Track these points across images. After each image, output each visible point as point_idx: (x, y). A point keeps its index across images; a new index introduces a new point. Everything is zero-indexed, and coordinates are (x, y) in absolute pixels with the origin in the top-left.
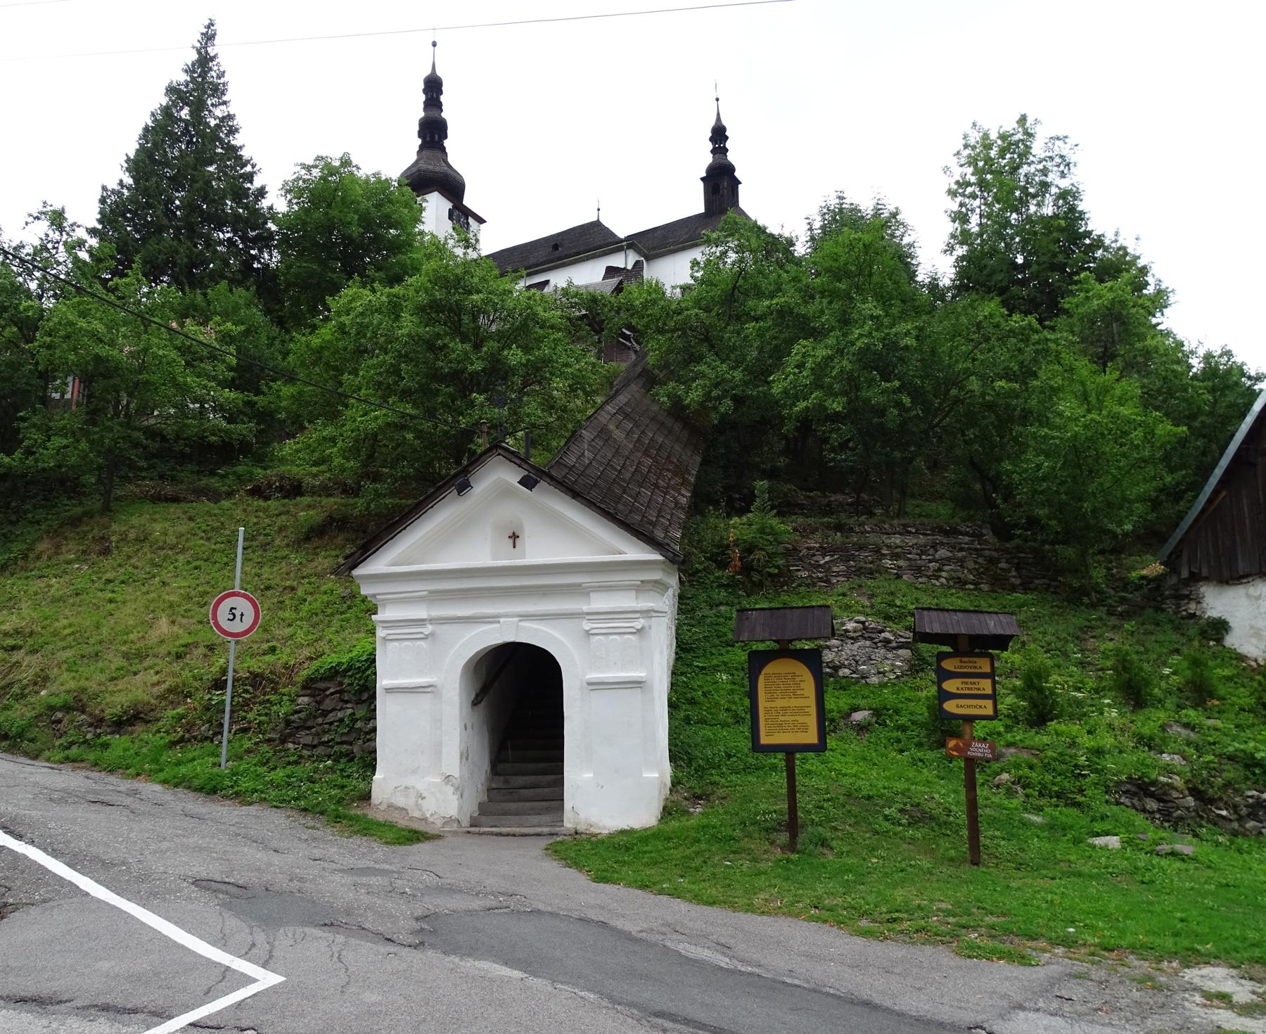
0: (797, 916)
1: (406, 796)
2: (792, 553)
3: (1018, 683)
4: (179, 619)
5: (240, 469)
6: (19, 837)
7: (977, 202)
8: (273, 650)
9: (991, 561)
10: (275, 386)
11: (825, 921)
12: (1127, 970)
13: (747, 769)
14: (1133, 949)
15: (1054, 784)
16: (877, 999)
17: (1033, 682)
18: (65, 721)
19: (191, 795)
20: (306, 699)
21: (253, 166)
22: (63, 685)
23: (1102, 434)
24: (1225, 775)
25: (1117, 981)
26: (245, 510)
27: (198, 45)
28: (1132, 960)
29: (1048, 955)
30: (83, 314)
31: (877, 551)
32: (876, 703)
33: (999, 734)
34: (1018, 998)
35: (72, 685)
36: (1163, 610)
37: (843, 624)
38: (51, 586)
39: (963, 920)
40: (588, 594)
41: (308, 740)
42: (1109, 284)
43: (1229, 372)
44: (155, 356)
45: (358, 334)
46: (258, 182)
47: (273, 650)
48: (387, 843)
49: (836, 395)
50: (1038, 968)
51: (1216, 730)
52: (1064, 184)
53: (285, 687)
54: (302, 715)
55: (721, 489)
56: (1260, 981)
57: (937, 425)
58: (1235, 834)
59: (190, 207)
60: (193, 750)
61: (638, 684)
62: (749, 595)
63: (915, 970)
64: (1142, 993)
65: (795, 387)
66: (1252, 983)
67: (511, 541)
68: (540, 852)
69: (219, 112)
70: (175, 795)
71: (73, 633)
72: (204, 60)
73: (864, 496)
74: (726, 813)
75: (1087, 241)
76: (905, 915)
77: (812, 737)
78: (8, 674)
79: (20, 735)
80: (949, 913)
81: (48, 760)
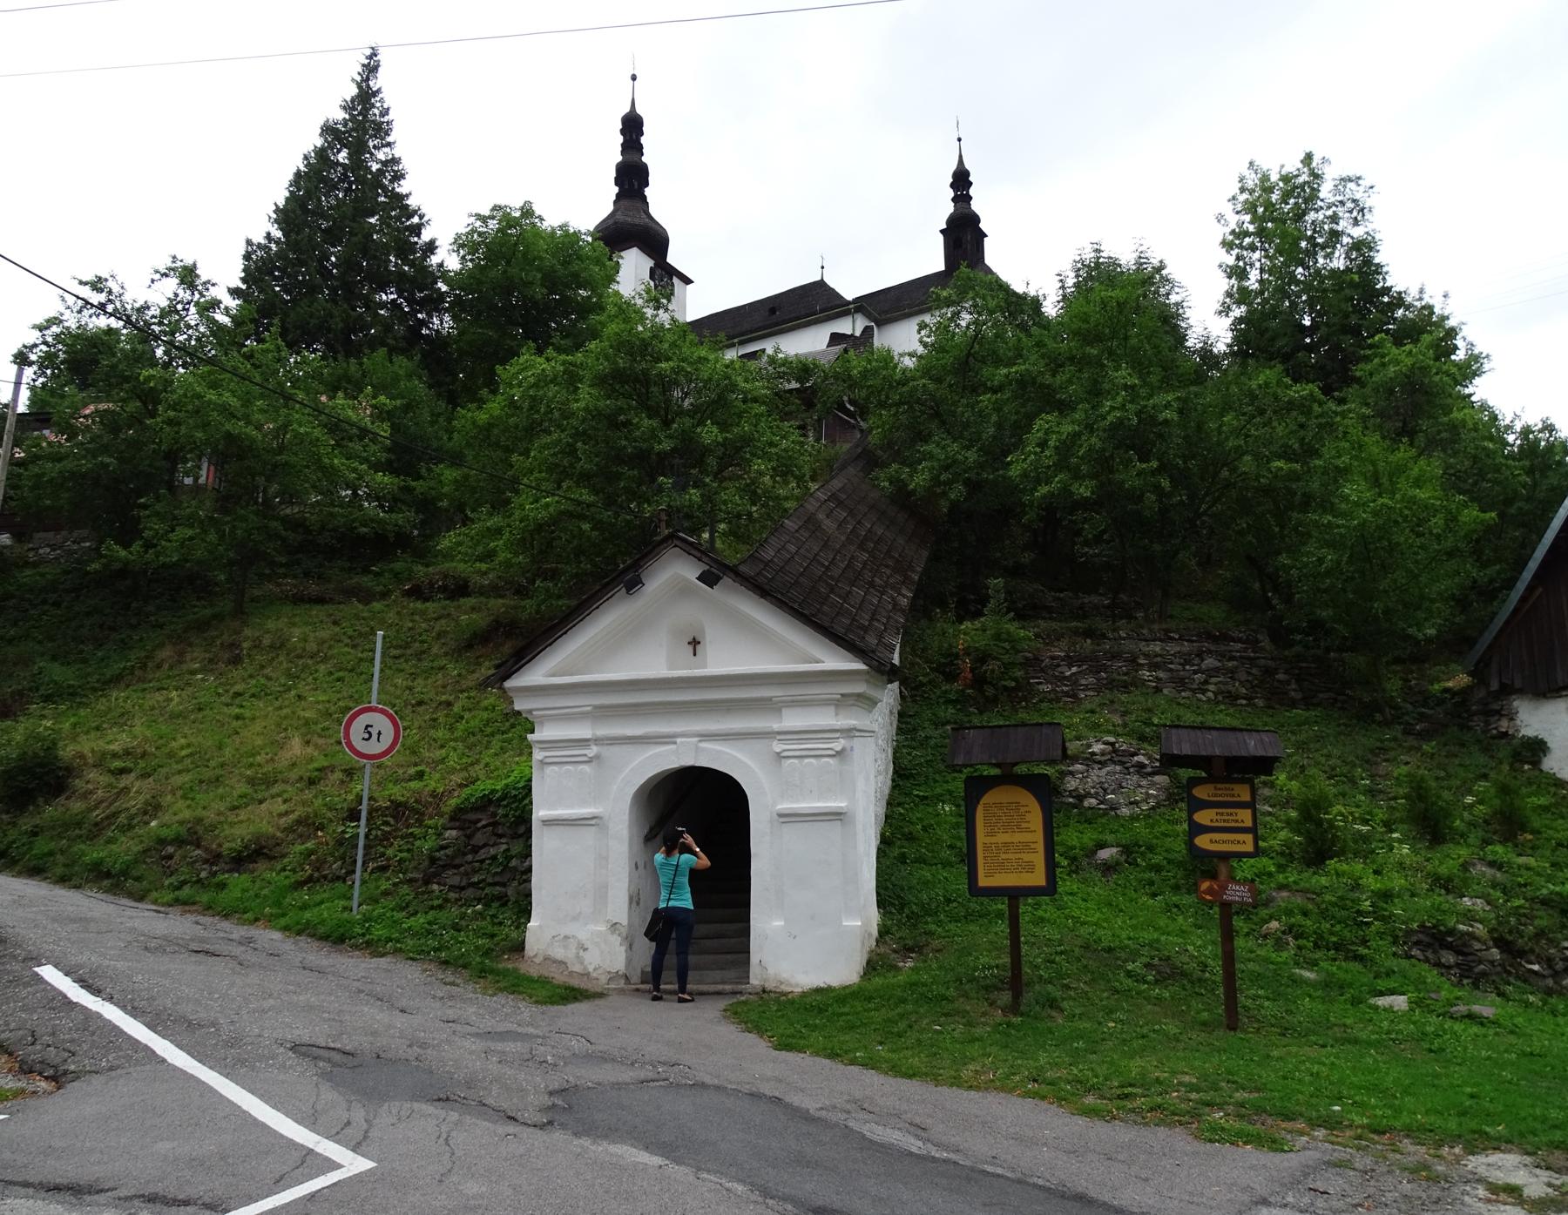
0: (1011, 1091)
1: (565, 947)
2: (1033, 663)
3: (1293, 814)
4: (315, 738)
5: (398, 566)
6: (96, 991)
7: (1257, 255)
8: (420, 775)
9: (1268, 672)
10: (438, 469)
11: (1043, 1098)
12: (1398, 1156)
13: (969, 917)
14: (1409, 1132)
15: (1332, 934)
16: (1093, 1194)
17: (1311, 813)
18: (177, 857)
19: (316, 944)
20: (454, 833)
21: (421, 217)
22: (177, 814)
23: (1396, 522)
24: (1536, 922)
25: (1385, 1169)
26: (398, 613)
27: (359, 78)
28: (1407, 1145)
29: (1305, 1138)
30: (214, 385)
31: (1133, 660)
32: (1125, 838)
33: (1270, 875)
34: (1261, 1190)
35: (187, 814)
36: (1470, 728)
37: (1089, 746)
38: (172, 700)
39: (1207, 1097)
40: (779, 710)
41: (456, 880)
42: (1408, 347)
43: (1551, 447)
44: (296, 435)
45: (531, 408)
46: (426, 236)
47: (420, 775)
48: (537, 1002)
49: (1083, 478)
50: (1292, 1155)
51: (1528, 868)
52: (1358, 232)
53: (431, 818)
54: (449, 852)
55: (948, 590)
56: (1559, 1171)
57: (1205, 513)
58: (1549, 992)
59: (347, 264)
60: (323, 892)
61: (837, 816)
62: (981, 713)
63: (1142, 1157)
64: (1415, 1185)
65: (1036, 469)
66: (1548, 1173)
67: (691, 648)
68: (718, 1014)
69: (381, 155)
70: (295, 943)
71: (191, 755)
72: (366, 96)
73: (1124, 597)
74: (940, 968)
75: (1386, 299)
76: (1140, 1091)
77: (1038, 878)
78: (115, 801)
79: (125, 873)
80: (1193, 1088)
81: (155, 902)
